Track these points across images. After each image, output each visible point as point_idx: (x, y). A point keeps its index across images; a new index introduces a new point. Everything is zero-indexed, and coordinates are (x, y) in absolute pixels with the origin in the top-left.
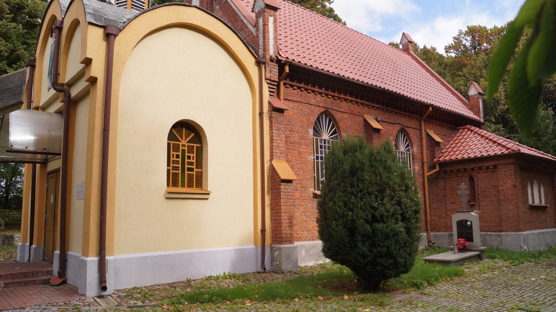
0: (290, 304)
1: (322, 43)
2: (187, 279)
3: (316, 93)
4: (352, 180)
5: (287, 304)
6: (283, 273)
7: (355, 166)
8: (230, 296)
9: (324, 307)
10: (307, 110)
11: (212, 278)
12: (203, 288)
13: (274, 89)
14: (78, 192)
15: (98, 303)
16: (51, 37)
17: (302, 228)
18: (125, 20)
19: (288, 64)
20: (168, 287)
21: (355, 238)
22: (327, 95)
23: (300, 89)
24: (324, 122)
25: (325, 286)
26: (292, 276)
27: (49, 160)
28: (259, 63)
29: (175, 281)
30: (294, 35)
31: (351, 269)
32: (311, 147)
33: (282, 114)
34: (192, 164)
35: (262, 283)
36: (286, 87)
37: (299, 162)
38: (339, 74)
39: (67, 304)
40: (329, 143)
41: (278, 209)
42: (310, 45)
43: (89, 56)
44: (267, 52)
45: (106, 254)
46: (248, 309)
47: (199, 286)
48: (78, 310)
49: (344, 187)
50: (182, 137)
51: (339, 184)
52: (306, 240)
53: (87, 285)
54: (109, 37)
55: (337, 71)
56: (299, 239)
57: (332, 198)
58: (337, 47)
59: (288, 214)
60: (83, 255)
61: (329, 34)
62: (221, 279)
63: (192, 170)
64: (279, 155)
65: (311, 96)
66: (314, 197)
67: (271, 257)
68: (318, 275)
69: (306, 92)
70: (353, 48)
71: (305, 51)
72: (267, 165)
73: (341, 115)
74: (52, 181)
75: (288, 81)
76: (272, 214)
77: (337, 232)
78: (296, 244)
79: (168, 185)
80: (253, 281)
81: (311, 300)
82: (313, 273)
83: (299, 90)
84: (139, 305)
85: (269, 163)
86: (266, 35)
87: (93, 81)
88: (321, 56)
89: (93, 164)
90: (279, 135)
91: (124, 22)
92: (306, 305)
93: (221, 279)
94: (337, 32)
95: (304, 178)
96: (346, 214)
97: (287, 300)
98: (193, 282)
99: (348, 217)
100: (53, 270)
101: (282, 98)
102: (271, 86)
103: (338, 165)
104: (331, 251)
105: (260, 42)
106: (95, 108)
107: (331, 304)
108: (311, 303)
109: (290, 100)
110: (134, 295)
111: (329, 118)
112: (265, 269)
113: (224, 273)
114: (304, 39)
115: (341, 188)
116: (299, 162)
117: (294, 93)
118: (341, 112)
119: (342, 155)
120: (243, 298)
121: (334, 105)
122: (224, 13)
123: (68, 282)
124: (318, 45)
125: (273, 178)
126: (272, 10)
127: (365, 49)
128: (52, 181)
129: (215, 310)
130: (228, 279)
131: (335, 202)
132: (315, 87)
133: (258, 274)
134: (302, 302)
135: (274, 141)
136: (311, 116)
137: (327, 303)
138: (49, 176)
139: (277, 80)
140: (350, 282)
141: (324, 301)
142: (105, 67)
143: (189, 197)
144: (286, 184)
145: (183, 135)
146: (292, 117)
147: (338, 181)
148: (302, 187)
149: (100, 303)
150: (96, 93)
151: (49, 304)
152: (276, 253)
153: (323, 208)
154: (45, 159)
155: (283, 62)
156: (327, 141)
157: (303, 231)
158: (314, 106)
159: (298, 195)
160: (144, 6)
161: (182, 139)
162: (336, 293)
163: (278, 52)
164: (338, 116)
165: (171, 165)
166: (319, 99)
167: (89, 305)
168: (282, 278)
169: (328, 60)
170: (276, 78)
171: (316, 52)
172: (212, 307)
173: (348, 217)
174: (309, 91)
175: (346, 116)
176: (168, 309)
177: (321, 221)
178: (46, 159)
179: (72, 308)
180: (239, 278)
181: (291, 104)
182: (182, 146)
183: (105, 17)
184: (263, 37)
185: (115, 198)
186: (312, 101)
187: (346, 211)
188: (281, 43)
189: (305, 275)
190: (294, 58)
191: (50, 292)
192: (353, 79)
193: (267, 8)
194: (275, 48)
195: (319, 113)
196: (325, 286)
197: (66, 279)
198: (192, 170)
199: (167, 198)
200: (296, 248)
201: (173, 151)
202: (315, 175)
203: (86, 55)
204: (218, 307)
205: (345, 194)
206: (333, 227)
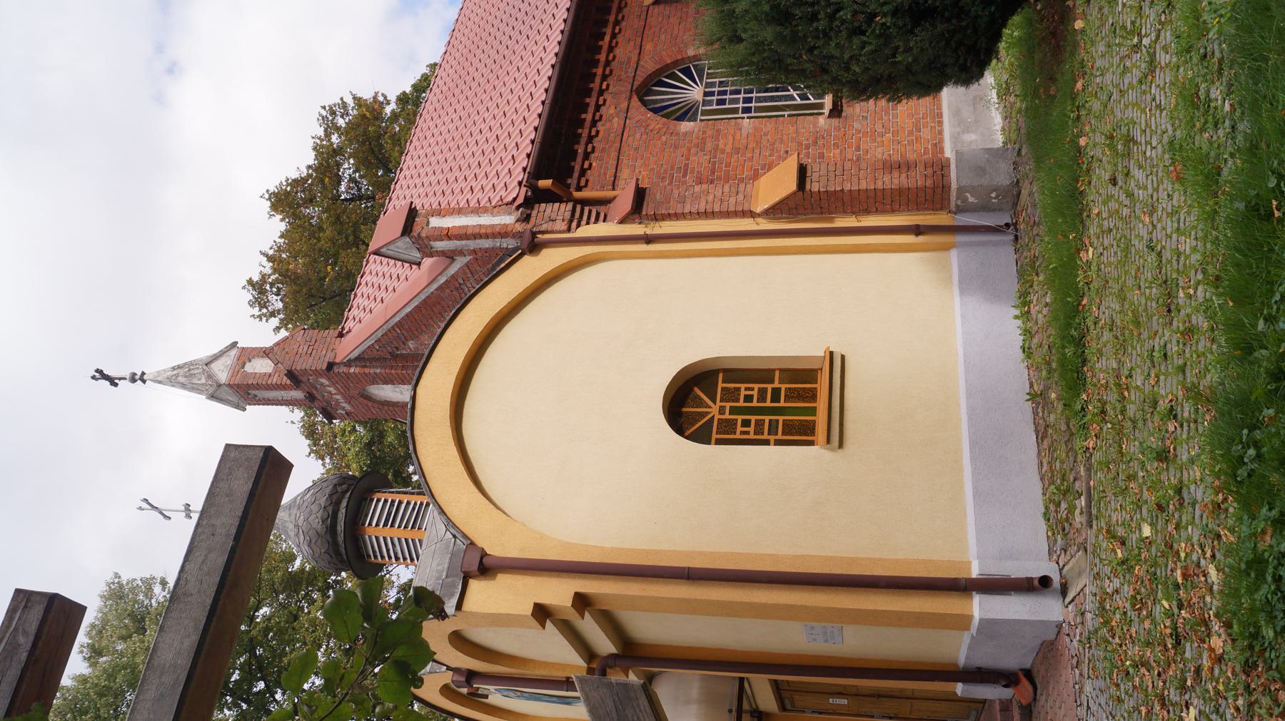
0: (1092, 157)
1: (482, 109)
2: (1028, 400)
3: (597, 118)
4: (801, 18)
5: (1091, 162)
6: (1018, 182)
7: (767, 14)
8: (1070, 296)
9: (1102, 75)
10: (638, 136)
11: (1027, 346)
12: (1048, 363)
13: (590, 212)
14: (826, 641)
15: (1079, 594)
16: (486, 697)
18: (449, 535)
19: (533, 181)
20: (1045, 442)
21: (938, 7)
22: (601, 92)
23: (596, 121)
24: (663, 96)
25: (1051, 78)
26: (1025, 160)
27: (754, 706)
28: (534, 246)
29: (1033, 427)
30: (467, 173)
31: (1013, 14)
32: (721, 126)
33: (647, 191)
34: (762, 393)
35: (1042, 229)
36: (586, 185)
37: (757, 151)
38: (553, 66)
39: (1078, 662)
40: (713, 85)
41: (868, 197)
42: (489, 135)
43: (528, 610)
44: (509, 229)
45: (965, 576)
46: (1101, 254)
47: (1044, 373)
48: (1091, 636)
49: (817, 38)
50: (704, 415)
51: (811, 50)
52: (941, 132)
53: (1037, 619)
54: (486, 567)
55: (545, 71)
56: (938, 147)
57: (843, 65)
58: (491, 75)
59: (879, 174)
60: (967, 628)
61: (461, 96)
62: (1029, 325)
63: (776, 392)
64: (741, 197)
65: (604, 128)
66: (839, 116)
67: (979, 211)
68: (1024, 97)
69: (596, 140)
70: (490, 39)
71: (502, 146)
72: (765, 225)
73: (646, 58)
74: (800, 700)
75: (573, 182)
76: (878, 211)
77: (922, 49)
78: (949, 153)
79: (811, 443)
80: (1037, 249)
81: (1083, 106)
82: (1019, 111)
83: (593, 155)
84: (1086, 502)
85: (759, 220)
86: (470, 232)
87: (582, 602)
88: (513, 110)
89: (763, 601)
90: (696, 198)
91: (454, 536)
92: (1097, 117)
93: (1029, 325)
94: (456, 77)
96: (880, 30)
97: (1083, 163)
98: (1036, 387)
99: (888, 24)
100: (1000, 700)
101: (610, 194)
102: (585, 218)
103: (765, 55)
104: (969, 64)
105: (487, 246)
106: (641, 597)
107: (1094, 59)
108: (1091, 106)
109: (615, 177)
110: (1061, 517)
111: (655, 85)
112: (1007, 225)
113: (1016, 317)
114: (475, 149)
115: (820, 43)
116: (757, 151)
117: (600, 166)
118: (639, 60)
119: (742, 46)
120: (1076, 267)
121: (624, 76)
122: (424, 329)
123: (1028, 666)
124: (481, 139)
125: (794, 211)
126: (414, 221)
127: (492, 10)
128: (800, 700)
129: (1102, 328)
130: (1029, 307)
131: (851, 58)
132: (584, 120)
133: (1020, 241)
134: (1087, 128)
135: (709, 210)
136: (651, 127)
137: (1092, 67)
138: (789, 707)
139: (570, 205)
140: (1042, 20)
141: (1086, 77)
142: (551, 577)
143: (839, 386)
144: (808, 180)
145: (699, 413)
147: (803, 52)
148: (815, 143)
149: (1078, 589)
150: (608, 595)
151: (1078, 700)
152: (971, 199)
153: (867, 87)
154: (751, 716)
155: (529, 193)
156: (707, 90)
158: (627, 121)
159: (834, 153)
160: (415, 504)
161: (708, 413)
162: (1068, 49)
163: (507, 204)
164: (649, 66)
165: (765, 436)
166: (612, 111)
167: (1083, 614)
168: (1031, 184)
169: (521, 93)
170: (566, 209)
171: (503, 120)
172: (1095, 336)
173: (888, 24)
174: (593, 133)
175: (648, 47)
176: (1096, 435)
177: (897, 90)
178: (751, 712)
179: (1087, 650)
180: (1028, 282)
181: (625, 173)
182: (724, 413)
183: (444, 577)
184: (475, 238)
185: (841, 557)
187: (874, 31)
188: (487, 199)
189: (1023, 131)
190: (520, 169)
191: (1050, 703)
192: (562, 32)
193: (411, 231)
194: (498, 212)
195: (643, 109)
196: (1051, 78)
197: (1021, 670)
198: (776, 392)
199: (841, 445)
200: (959, 154)
201: (735, 433)
202: (786, 113)
203: (526, 616)
204: (1095, 324)
205: (832, 34)
206: (910, 59)
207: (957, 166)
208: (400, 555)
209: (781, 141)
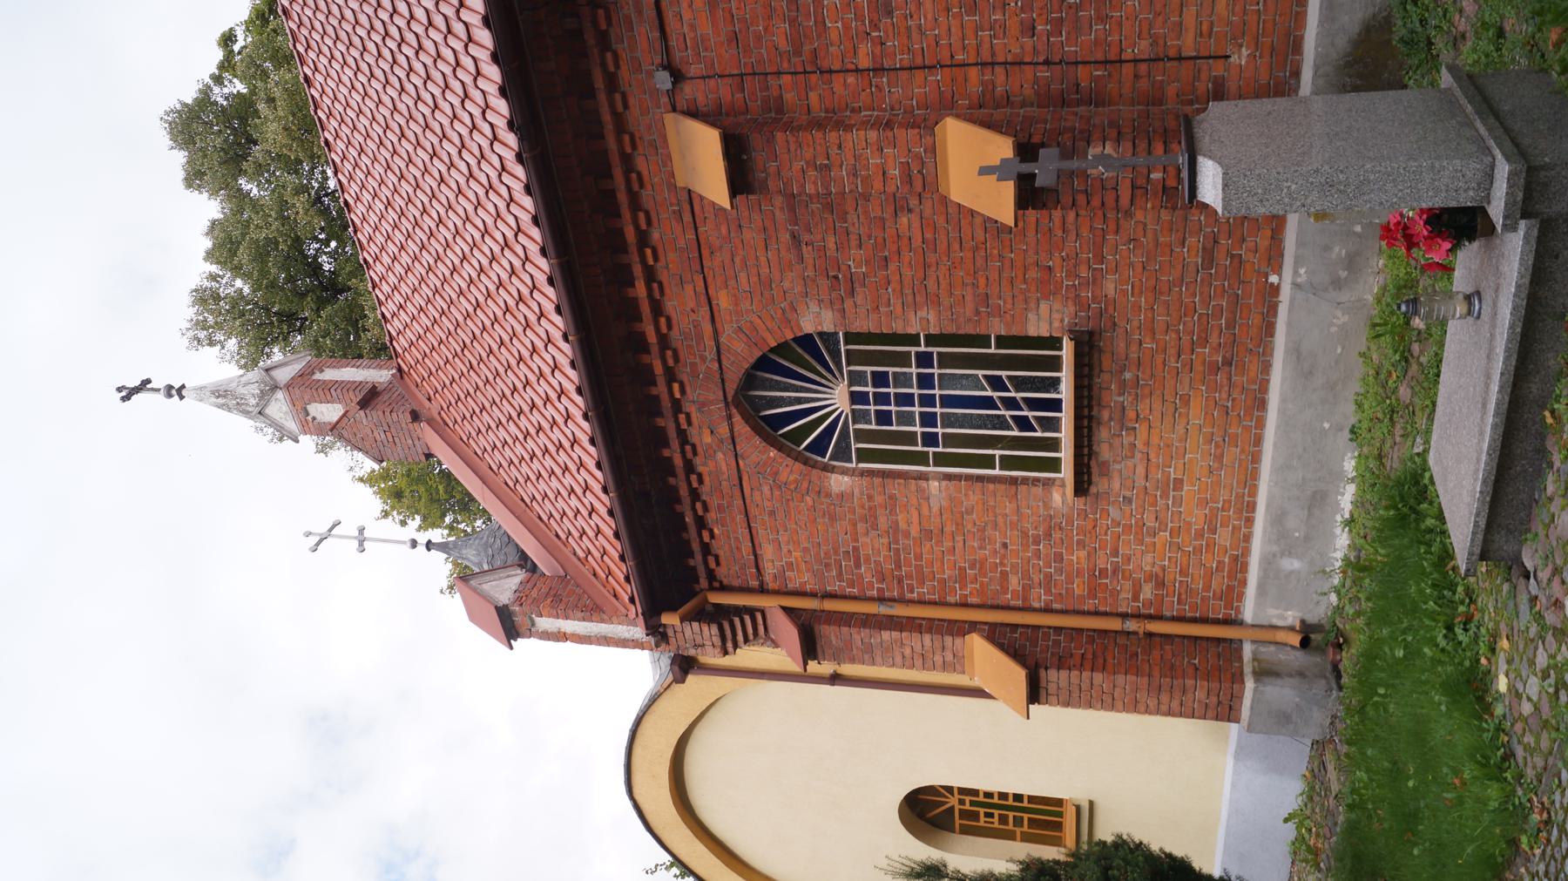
24: (785, 397)
37: (959, 538)
52: (1248, 538)
95: (1013, 525)
102: (740, 637)
116: (959, 538)
146: (805, 550)
148: (1048, 535)
157: (1210, 545)
175: (723, 301)
186: (724, 468)
207: (1252, 708)
209: (995, 526)
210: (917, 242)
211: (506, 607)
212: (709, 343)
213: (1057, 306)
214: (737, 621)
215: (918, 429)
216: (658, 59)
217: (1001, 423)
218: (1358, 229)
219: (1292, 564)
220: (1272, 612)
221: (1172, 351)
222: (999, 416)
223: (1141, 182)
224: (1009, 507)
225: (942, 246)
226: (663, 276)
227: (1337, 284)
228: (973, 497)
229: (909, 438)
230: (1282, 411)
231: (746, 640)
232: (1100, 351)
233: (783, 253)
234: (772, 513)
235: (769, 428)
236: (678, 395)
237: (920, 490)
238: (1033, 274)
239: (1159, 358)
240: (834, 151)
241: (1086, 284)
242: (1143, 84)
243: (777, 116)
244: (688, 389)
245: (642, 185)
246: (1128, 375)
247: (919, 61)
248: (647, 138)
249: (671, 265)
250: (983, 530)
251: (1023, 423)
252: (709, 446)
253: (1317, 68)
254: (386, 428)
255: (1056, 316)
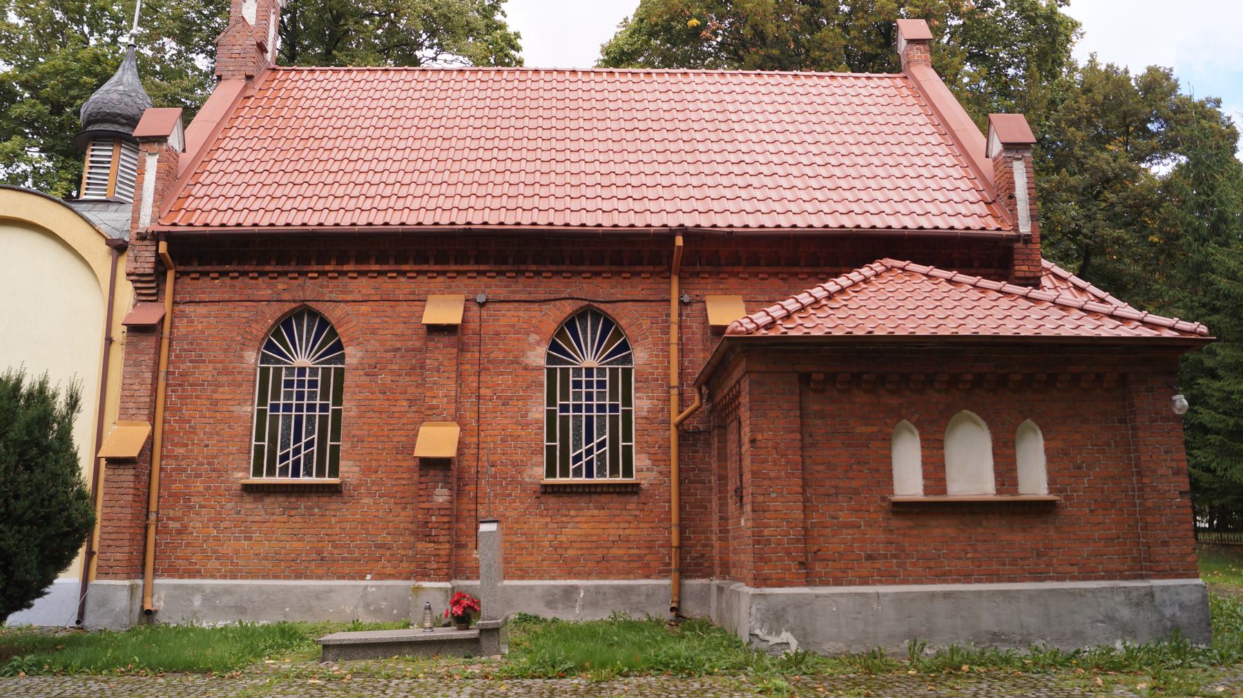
10: (246, 314)
17: (204, 551)
37: (211, 421)
102: (139, 285)
116: (211, 421)
136: (254, 325)
146: (203, 332)
157: (208, 558)
175: (364, 308)
186: (261, 293)
208: (93, 171)
210: (394, 409)
211: (166, 141)
212: (341, 297)
213: (356, 475)
214: (154, 285)
215: (282, 402)
216: (490, 297)
217: (285, 445)
218: (395, 612)
219: (197, 602)
220: (163, 594)
221: (330, 531)
222: (289, 444)
223: (431, 512)
224: (234, 449)
225: (391, 421)
226: (380, 279)
227: (367, 606)
228: (239, 430)
229: (276, 396)
230: (296, 587)
231: (136, 288)
232: (330, 497)
233: (390, 343)
234: (229, 316)
235: (286, 322)
236: (310, 275)
237: (245, 401)
238: (374, 464)
239: (326, 525)
240: (446, 375)
241: (368, 489)
242: (466, 513)
243: (462, 349)
244: (312, 281)
245: (429, 278)
246: (316, 510)
247: (481, 416)
248: (453, 284)
249: (386, 284)
250: (217, 434)
251: (285, 457)
252: (276, 287)
253: (470, 586)
254: (242, 55)
255: (351, 475)
